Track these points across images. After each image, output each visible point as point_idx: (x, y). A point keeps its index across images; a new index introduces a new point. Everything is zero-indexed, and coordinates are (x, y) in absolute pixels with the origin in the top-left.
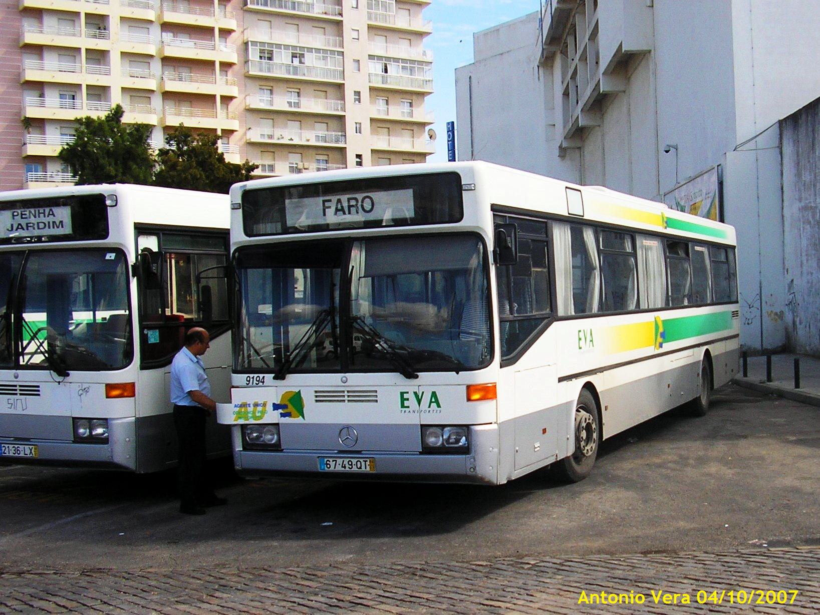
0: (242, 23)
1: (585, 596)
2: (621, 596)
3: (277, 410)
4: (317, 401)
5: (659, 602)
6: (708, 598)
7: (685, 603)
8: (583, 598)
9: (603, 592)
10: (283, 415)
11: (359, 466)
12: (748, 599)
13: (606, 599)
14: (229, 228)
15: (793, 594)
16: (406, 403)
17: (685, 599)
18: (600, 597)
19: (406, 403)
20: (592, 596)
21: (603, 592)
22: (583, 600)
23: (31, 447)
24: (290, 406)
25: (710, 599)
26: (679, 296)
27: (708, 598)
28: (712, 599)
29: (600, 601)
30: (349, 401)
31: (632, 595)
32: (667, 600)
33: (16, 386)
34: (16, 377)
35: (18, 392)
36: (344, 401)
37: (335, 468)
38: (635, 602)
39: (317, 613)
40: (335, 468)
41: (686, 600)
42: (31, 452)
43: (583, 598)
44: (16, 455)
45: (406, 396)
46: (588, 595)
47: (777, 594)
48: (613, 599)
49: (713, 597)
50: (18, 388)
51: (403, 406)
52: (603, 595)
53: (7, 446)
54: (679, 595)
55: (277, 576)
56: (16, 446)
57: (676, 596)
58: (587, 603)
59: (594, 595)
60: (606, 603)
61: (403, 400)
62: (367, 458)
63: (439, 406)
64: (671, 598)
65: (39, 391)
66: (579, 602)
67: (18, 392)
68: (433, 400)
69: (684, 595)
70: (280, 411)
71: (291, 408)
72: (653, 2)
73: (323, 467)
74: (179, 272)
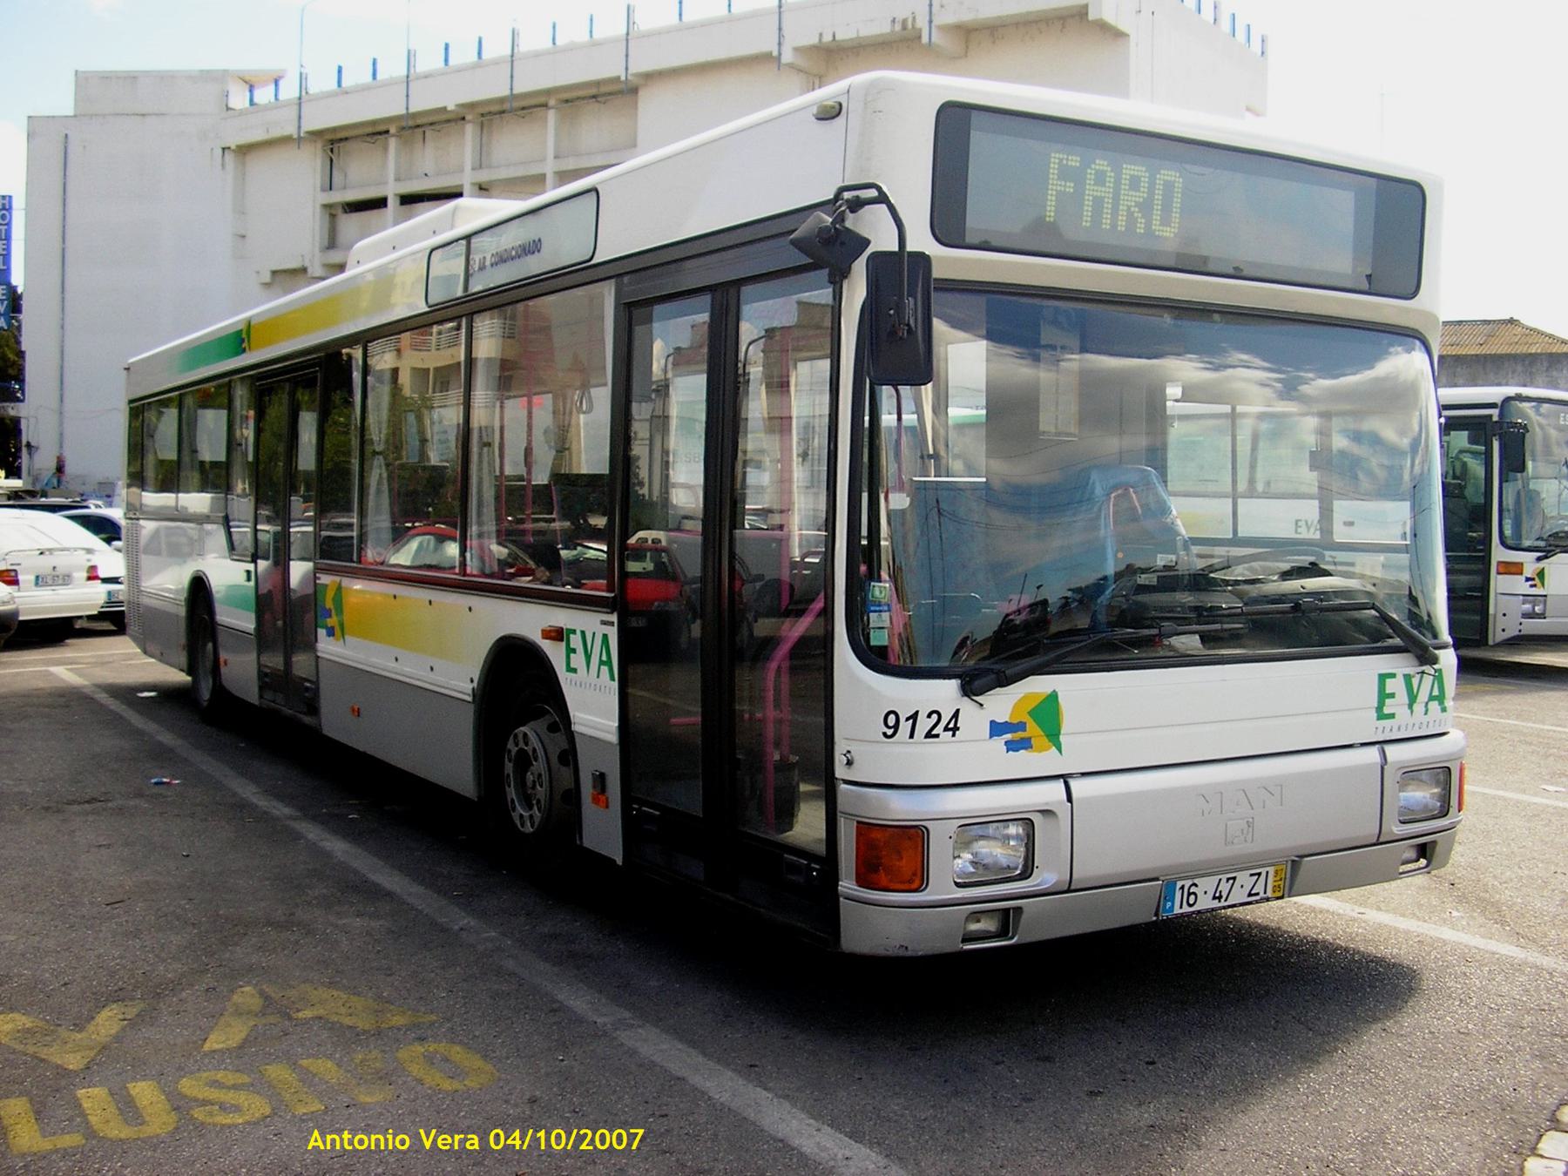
0: (936, 624)
1: (319, 1139)
6: (506, 1140)
7: (472, 1148)
8: (316, 1141)
9: (346, 1132)
10: (1532, 586)
12: (567, 1144)
13: (351, 1142)
14: (886, 643)
16: (1299, 530)
17: (472, 1142)
18: (342, 1140)
19: (1299, 530)
20: (329, 1137)
22: (316, 1144)
24: (1537, 579)
25: (509, 1142)
28: (513, 1142)
31: (390, 1137)
32: (444, 1145)
38: (394, 1146)
39: (742, 563)
43: (316, 1141)
45: (1300, 524)
46: (323, 1135)
47: (611, 1135)
48: (361, 1142)
49: (514, 1139)
52: (346, 1136)
54: (462, 1136)
55: (909, 418)
57: (457, 1137)
58: (322, 1147)
59: (378, 1136)
60: (351, 1148)
64: (450, 1141)
66: (310, 1148)
68: (951, 725)
69: (469, 1136)
71: (1537, 581)
74: (825, 655)
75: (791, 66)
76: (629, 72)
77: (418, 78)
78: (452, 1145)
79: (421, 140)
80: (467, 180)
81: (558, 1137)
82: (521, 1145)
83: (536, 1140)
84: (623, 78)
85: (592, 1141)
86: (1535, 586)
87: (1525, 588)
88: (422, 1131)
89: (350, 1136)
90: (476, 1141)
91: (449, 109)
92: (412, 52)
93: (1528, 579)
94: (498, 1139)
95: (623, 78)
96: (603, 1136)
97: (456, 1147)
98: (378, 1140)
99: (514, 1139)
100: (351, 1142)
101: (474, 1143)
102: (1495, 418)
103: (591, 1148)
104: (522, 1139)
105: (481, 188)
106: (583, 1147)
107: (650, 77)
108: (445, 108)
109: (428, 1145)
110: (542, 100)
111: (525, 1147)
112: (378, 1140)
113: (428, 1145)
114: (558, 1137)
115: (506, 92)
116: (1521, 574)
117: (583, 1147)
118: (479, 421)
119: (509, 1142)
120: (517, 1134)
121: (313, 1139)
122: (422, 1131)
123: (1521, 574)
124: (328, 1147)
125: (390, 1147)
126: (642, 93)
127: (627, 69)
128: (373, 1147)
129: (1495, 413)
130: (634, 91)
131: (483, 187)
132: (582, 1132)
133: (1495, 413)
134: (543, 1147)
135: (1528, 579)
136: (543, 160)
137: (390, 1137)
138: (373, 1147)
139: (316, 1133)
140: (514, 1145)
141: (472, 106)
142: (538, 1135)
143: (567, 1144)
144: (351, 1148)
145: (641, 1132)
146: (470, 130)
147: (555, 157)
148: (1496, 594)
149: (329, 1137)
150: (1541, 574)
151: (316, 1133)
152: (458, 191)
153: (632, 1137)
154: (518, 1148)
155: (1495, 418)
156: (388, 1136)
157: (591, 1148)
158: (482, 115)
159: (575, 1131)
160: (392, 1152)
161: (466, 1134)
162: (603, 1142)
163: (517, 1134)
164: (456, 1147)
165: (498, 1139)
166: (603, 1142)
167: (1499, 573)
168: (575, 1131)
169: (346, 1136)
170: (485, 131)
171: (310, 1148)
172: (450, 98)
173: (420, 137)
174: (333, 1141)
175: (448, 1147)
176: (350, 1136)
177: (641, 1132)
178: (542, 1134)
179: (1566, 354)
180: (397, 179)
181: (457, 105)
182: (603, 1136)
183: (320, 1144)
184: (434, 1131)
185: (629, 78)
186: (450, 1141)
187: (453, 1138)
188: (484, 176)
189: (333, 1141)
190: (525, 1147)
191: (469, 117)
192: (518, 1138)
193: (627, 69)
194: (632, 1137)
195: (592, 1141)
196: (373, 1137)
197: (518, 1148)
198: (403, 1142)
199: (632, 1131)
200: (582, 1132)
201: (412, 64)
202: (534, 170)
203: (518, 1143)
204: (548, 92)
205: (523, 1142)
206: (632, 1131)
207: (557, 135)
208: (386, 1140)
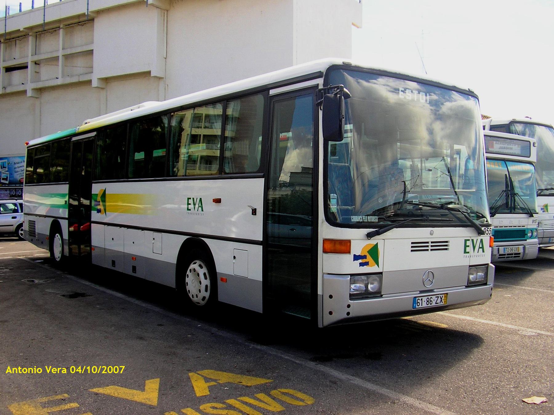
1: (10, 369)
2: (29, 369)
3: (357, 260)
4: (412, 251)
5: (50, 372)
6: (76, 370)
8: (9, 370)
9: (19, 367)
10: (361, 265)
11: (418, 305)
12: (98, 371)
15: (122, 368)
20: (13, 369)
21: (19, 367)
22: (9, 371)
23: (441, 296)
24: (369, 256)
26: (387, 164)
27: (76, 370)
28: (78, 371)
29: (36, 372)
30: (431, 250)
31: (35, 369)
33: (428, 243)
34: (431, 234)
35: (430, 248)
36: (427, 250)
37: (422, 305)
40: (422, 305)
41: (64, 371)
42: (441, 301)
43: (9, 370)
44: (429, 305)
48: (25, 371)
49: (79, 370)
50: (430, 244)
51: (465, 252)
52: (19, 368)
53: (420, 298)
54: (60, 369)
56: (429, 297)
57: (59, 369)
58: (11, 373)
60: (21, 373)
61: (466, 246)
62: (439, 294)
63: (483, 251)
64: (56, 370)
65: (412, 247)
66: (7, 373)
67: (430, 248)
69: (63, 369)
70: (360, 261)
71: (369, 259)
72: (33, 2)
73: (415, 305)
75: (152, 5)
76: (89, 11)
77: (9, 18)
78: (57, 372)
79: (14, 45)
80: (29, 60)
81: (94, 369)
82: (81, 372)
83: (86, 370)
84: (86, 14)
85: (106, 371)
86: (366, 264)
87: (355, 268)
88: (46, 367)
89: (21, 369)
90: (65, 370)
91: (21, 30)
92: (8, 7)
93: (356, 258)
94: (73, 370)
95: (86, 14)
96: (110, 368)
97: (58, 372)
98: (31, 370)
99: (79, 370)
100: (21, 370)
101: (65, 371)
102: (321, 87)
103: (106, 373)
104: (82, 369)
105: (36, 64)
106: (103, 372)
107: (99, 12)
108: (19, 30)
109: (48, 371)
110: (57, 25)
111: (83, 373)
112: (31, 370)
113: (48, 371)
114: (94, 369)
115: (42, 22)
116: (349, 252)
117: (103, 372)
118: (368, 178)
119: (77, 371)
120: (80, 368)
121: (8, 370)
122: (46, 367)
123: (349, 252)
124: (13, 372)
125: (35, 372)
126: (95, 20)
127: (88, 9)
128: (29, 372)
129: (320, 82)
130: (92, 20)
131: (37, 63)
132: (103, 367)
133: (320, 82)
134: (89, 372)
135: (356, 258)
136: (58, 51)
137: (35, 369)
138: (29, 372)
139: (9, 368)
140: (79, 372)
141: (31, 28)
142: (87, 368)
143: (98, 371)
144: (21, 373)
145: (124, 367)
146: (31, 39)
147: (63, 49)
148: (323, 274)
149: (13, 369)
150: (374, 252)
151: (9, 368)
152: (25, 65)
153: (120, 369)
154: (80, 373)
155: (321, 87)
156: (34, 368)
157: (106, 373)
158: (36, 33)
159: (100, 367)
160: (32, 374)
161: (62, 367)
162: (110, 371)
163: (80, 368)
164: (58, 372)
165: (73, 370)
166: (110, 371)
167: (325, 251)
168: (100, 367)
169: (19, 368)
170: (38, 39)
171: (7, 373)
172: (21, 25)
173: (14, 43)
174: (15, 370)
175: (55, 372)
176: (21, 369)
177: (124, 367)
178: (89, 368)
179: (553, 259)
180: (4, 61)
181: (25, 28)
182: (110, 368)
183: (10, 371)
184: (50, 367)
185: (89, 13)
186: (56, 370)
187: (57, 369)
188: (36, 58)
189: (15, 370)
190: (83, 373)
191: (30, 34)
192: (80, 369)
193: (88, 9)
194: (120, 369)
195: (106, 371)
196: (29, 369)
197: (80, 373)
198: (39, 371)
199: (120, 367)
200: (103, 367)
201: (8, 12)
202: (55, 55)
203: (80, 371)
204: (60, 21)
205: (82, 371)
206: (120, 367)
207: (63, 40)
208: (34, 370)
